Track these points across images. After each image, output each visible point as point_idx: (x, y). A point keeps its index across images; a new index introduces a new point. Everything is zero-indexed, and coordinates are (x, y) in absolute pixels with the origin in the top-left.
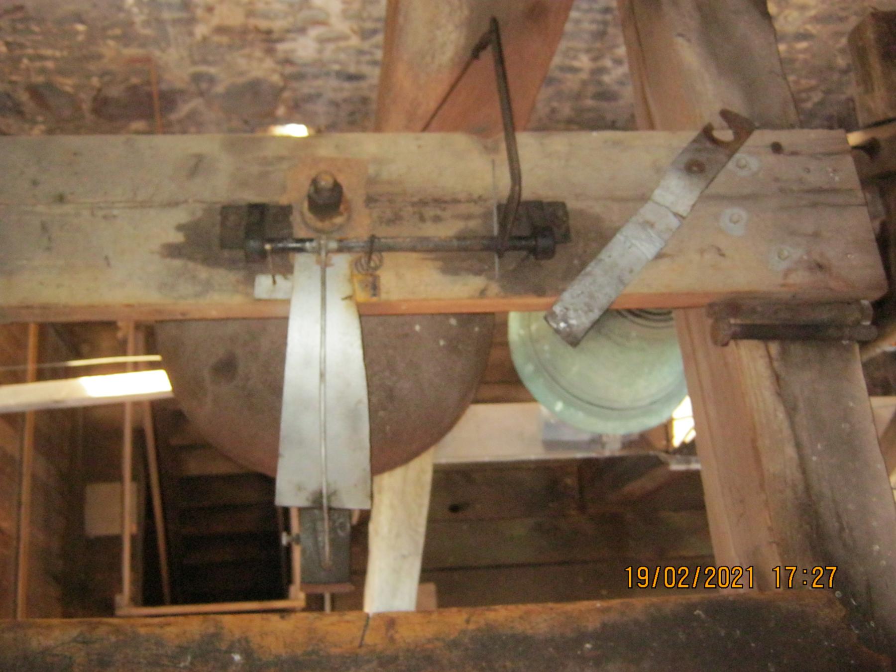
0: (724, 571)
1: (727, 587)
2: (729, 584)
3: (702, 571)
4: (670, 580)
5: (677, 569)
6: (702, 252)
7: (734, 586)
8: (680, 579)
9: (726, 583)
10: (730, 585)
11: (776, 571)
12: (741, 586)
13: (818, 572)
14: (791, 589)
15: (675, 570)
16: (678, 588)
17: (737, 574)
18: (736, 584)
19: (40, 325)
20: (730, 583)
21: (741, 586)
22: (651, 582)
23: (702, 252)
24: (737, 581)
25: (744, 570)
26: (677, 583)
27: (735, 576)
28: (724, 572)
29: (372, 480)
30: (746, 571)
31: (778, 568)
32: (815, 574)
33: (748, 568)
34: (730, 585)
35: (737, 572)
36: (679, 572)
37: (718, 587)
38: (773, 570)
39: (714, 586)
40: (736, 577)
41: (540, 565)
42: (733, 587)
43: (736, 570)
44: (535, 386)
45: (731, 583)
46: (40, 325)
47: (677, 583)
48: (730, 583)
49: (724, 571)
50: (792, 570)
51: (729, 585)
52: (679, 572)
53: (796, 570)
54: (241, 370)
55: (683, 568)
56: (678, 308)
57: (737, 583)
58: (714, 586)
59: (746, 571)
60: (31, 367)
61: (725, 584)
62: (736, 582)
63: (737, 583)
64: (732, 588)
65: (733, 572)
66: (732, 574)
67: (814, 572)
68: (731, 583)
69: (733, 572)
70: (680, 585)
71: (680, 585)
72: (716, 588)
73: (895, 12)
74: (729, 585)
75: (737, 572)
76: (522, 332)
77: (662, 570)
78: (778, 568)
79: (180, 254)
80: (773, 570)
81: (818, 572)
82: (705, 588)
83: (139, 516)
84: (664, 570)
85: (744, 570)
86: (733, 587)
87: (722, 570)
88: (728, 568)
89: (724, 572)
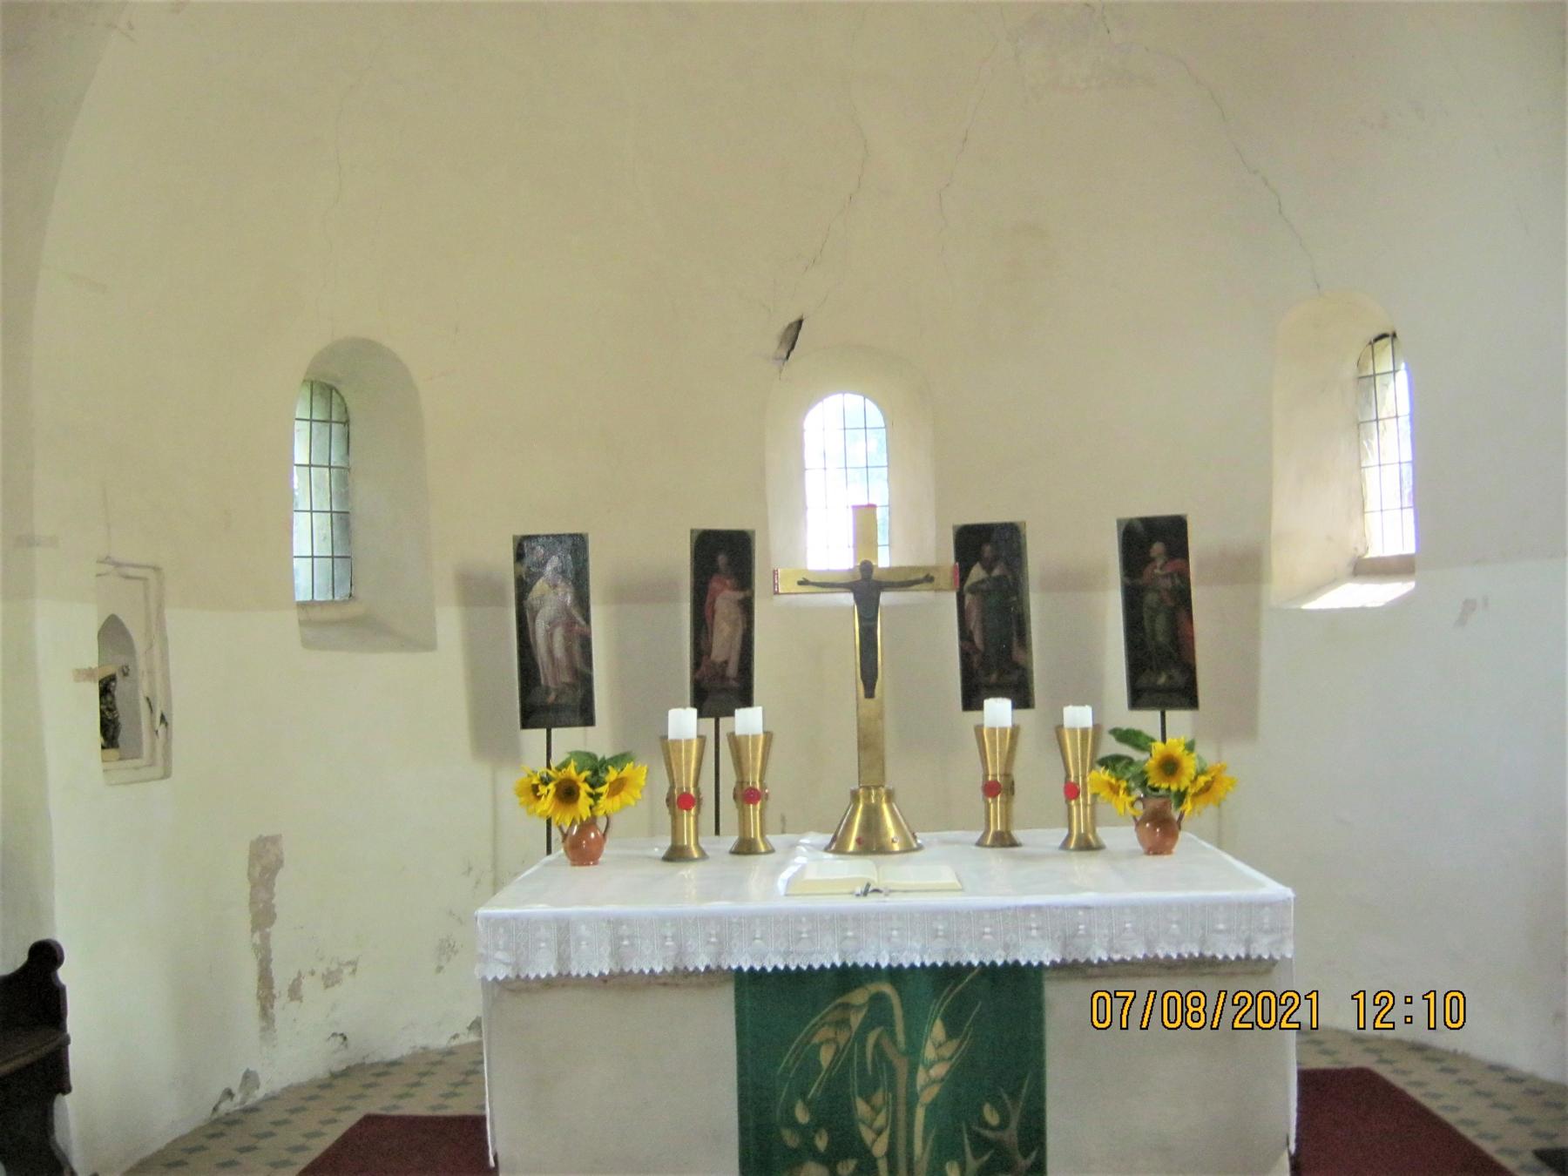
0: (1266, 1000)
1: (1273, 1027)
2: (1276, 1021)
7: (1284, 1025)
8: (1285, 1013)
9: (1176, 1020)
10: (1278, 1023)
11: (1358, 999)
12: (1391, 1026)
13: (1243, 1001)
14: (1410, 1025)
15: (1276, 998)
16: (1281, 1029)
17: (1289, 1004)
18: (1241, 1022)
21: (1391, 1026)
24: (1290, 1016)
25: (1303, 998)
27: (1286, 1007)
30: (1306, 999)
31: (1362, 994)
33: (1309, 994)
34: (1278, 1023)
37: (1255, 1026)
38: (1353, 998)
40: (1287, 1010)
41: (865, 146)
42: (1282, 1026)
45: (1279, 1021)
48: (1278, 1022)
49: (1266, 1000)
50: (1127, 998)
51: (1275, 1025)
53: (1135, 997)
56: (220, 1102)
59: (1306, 999)
61: (1268, 1022)
62: (1288, 1019)
63: (1243, 1020)
64: (1281, 1029)
65: (1283, 1002)
66: (1281, 1005)
67: (1236, 1002)
68: (1279, 1021)
69: (1283, 1002)
73: (1565, 1087)
74: (1275, 1025)
75: (1384, 1001)
78: (1362, 994)
80: (1353, 998)
86: (1282, 1026)
88: (1274, 994)
89: (1266, 1000)
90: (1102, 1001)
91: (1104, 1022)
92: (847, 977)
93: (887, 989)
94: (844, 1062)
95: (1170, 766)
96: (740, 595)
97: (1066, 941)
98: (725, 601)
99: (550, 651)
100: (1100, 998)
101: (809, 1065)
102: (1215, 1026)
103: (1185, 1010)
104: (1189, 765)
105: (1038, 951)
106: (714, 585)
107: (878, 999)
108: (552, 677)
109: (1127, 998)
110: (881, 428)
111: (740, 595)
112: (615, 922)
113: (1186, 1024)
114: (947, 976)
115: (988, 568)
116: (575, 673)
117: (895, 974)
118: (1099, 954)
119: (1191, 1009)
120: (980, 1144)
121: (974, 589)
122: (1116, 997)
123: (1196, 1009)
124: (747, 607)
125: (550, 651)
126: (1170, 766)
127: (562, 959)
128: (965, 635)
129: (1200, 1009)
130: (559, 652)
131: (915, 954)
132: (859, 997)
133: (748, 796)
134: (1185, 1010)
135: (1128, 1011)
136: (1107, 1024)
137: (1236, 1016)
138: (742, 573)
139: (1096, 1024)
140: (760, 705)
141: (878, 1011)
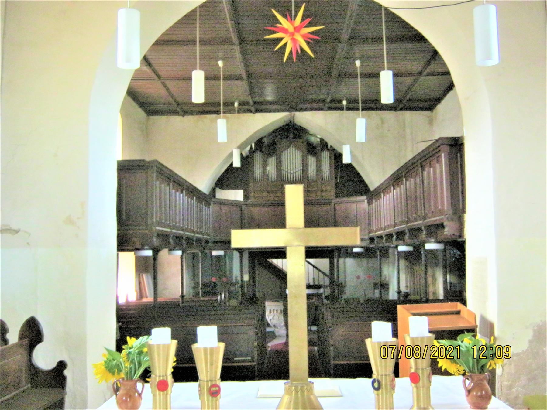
0: (442, 349)
3: (429, 349)
4: (442, 350)
6: (464, 370)
7: (448, 357)
18: (449, 356)
19: (474, 329)
20: (446, 356)
23: (464, 370)
25: (454, 348)
29: (319, 282)
35: (450, 349)
43: (449, 348)
46: (474, 329)
48: (446, 356)
50: (393, 348)
54: (461, 313)
57: (450, 356)
63: (450, 356)
64: (447, 359)
65: (448, 349)
69: (448, 349)
75: (450, 349)
85: (454, 348)
87: (385, 356)
103: (413, 352)
119: (416, 352)
134: (413, 352)
136: (497, 347)
137: (431, 354)
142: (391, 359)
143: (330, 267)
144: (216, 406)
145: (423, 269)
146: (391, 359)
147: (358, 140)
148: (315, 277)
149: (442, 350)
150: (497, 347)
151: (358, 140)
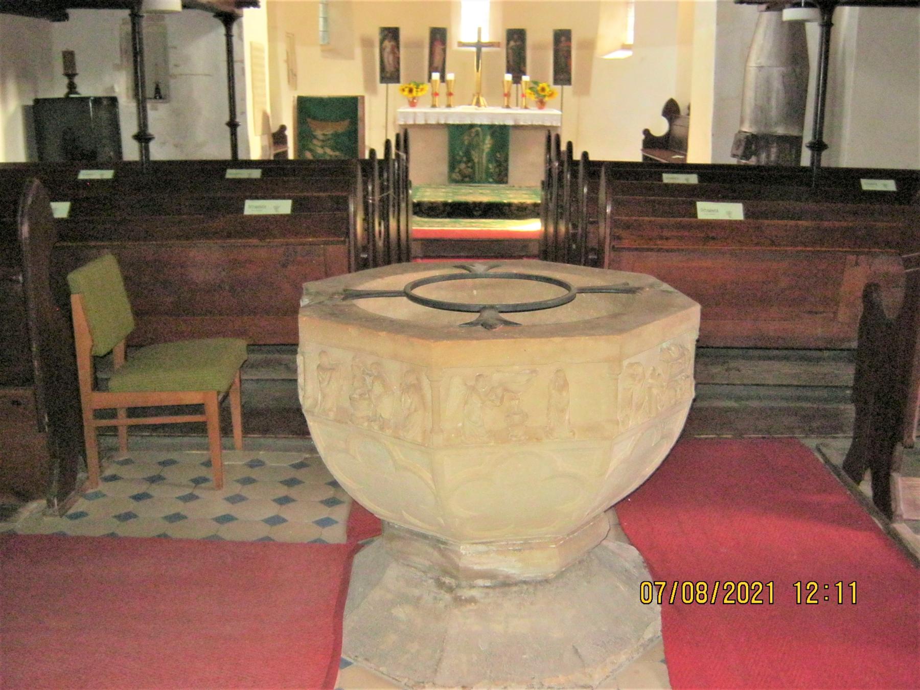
3: (721, 587)
4: (688, 595)
5: (750, 584)
8: (754, 595)
16: (807, 604)
22: (710, 596)
25: (764, 585)
26: (750, 599)
28: (646, 587)
32: (727, 589)
36: (753, 588)
39: (733, 602)
44: (304, 480)
47: (750, 599)
50: (661, 585)
52: (753, 588)
53: (666, 585)
55: (760, 584)
58: (733, 602)
60: (88, 115)
70: (753, 601)
71: (753, 601)
72: (735, 603)
76: (766, 160)
77: (680, 585)
79: (161, 98)
81: (812, 587)
82: (724, 603)
83: (191, 540)
84: (682, 585)
85: (764, 585)
90: (646, 587)
91: (648, 600)
92: (472, 126)
93: (479, 129)
94: (470, 145)
95: (543, 89)
96: (442, 47)
97: (515, 120)
98: (438, 49)
99: (388, 61)
100: (645, 585)
101: (463, 143)
102: (713, 602)
103: (695, 593)
104: (547, 89)
105: (510, 123)
106: (436, 43)
107: (477, 131)
108: (390, 68)
109: (661, 585)
110: (562, 90)
111: (442, 47)
112: (425, 113)
113: (696, 601)
114: (491, 127)
115: (515, 41)
116: (395, 68)
117: (481, 126)
118: (522, 123)
119: (699, 592)
120: (497, 161)
121: (512, 49)
122: (654, 585)
123: (702, 592)
124: (444, 51)
125: (388, 61)
126: (543, 89)
127: (415, 121)
128: (508, 62)
129: (704, 592)
130: (391, 62)
131: (486, 122)
132: (473, 130)
133: (450, 94)
134: (695, 593)
135: (662, 593)
136: (650, 601)
137: (725, 596)
138: (444, 42)
139: (643, 601)
140: (452, 72)
141: (477, 134)
142: (658, 603)
143: (422, 285)
144: (505, 7)
145: (672, 402)
146: (658, 603)
147: (248, 203)
148: (389, 138)
149: (688, 595)
150: (650, 601)
151: (248, 203)
